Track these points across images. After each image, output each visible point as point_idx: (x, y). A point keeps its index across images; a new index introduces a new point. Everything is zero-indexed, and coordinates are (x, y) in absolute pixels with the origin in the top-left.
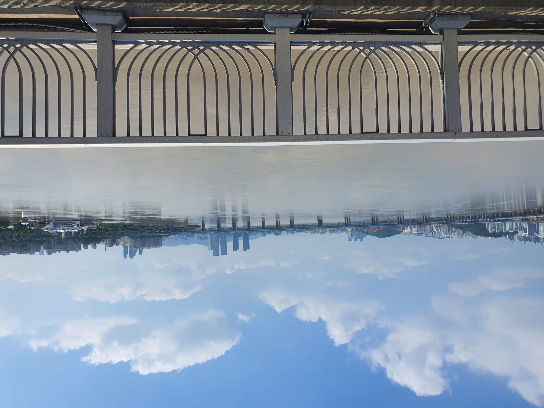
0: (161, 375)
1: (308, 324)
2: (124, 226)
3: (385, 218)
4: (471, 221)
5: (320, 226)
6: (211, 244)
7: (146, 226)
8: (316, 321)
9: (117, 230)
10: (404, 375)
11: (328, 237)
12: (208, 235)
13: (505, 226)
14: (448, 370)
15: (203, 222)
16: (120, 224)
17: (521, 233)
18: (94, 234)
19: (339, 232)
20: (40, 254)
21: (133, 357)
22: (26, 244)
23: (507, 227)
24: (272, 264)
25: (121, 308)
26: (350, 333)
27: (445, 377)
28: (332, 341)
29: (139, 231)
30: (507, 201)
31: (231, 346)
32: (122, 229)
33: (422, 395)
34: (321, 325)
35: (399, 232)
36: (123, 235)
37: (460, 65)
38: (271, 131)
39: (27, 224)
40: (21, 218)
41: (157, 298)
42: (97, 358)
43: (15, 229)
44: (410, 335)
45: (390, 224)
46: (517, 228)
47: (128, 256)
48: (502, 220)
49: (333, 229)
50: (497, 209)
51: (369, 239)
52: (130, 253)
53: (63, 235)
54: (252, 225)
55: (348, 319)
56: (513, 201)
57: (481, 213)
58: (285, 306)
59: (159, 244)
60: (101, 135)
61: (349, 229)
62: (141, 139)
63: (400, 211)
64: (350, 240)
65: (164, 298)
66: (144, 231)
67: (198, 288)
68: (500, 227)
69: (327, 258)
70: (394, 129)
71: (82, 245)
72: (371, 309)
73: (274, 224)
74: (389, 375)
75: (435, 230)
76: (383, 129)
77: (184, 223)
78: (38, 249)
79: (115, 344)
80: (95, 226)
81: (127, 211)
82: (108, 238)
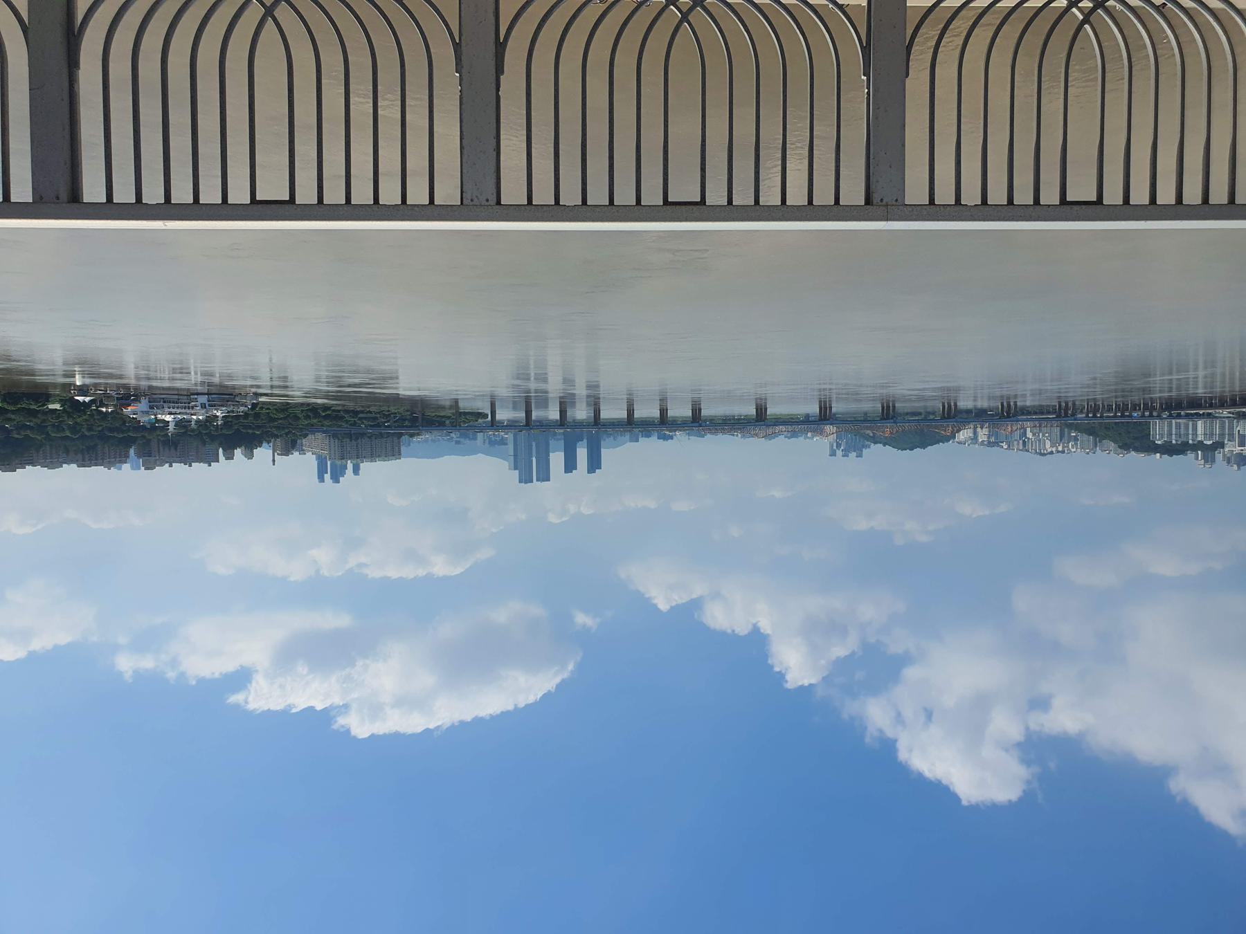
0: (396, 737)
1: (726, 640)
2: (313, 410)
3: (916, 405)
4: (1115, 416)
5: (760, 420)
6: (515, 456)
7: (362, 412)
8: (746, 632)
9: (297, 418)
10: (939, 759)
11: (781, 446)
12: (509, 436)
13: (1195, 428)
14: (1034, 748)
15: (493, 405)
16: (302, 404)
17: (1232, 447)
18: (245, 427)
19: (809, 435)
20: (133, 468)
21: (337, 700)
22: (96, 445)
23: (1199, 432)
24: (652, 504)
25: (315, 591)
26: (823, 662)
27: (1027, 762)
28: (781, 676)
29: (347, 422)
30: (1205, 368)
31: (558, 680)
32: (308, 417)
33: (973, 801)
34: (757, 641)
35: (946, 439)
36: (312, 429)
37: (909, 48)
38: (853, 194)
39: (87, 399)
40: (75, 385)
41: (393, 573)
42: (263, 697)
43: (64, 411)
44: (958, 668)
45: (925, 419)
46: (1222, 435)
47: (327, 477)
48: (1187, 416)
49: (797, 428)
50: (1179, 389)
51: (877, 452)
52: (331, 470)
53: (171, 427)
54: (606, 414)
55: (818, 630)
56: (1219, 371)
57: (1136, 398)
58: (679, 598)
59: (395, 453)
60: (41, 198)
61: (829, 428)
62: (348, 210)
63: (949, 389)
64: (833, 454)
65: (409, 572)
66: (360, 423)
67: (485, 553)
68: (1182, 431)
69: (777, 494)
70: (1140, 196)
71: (221, 450)
72: (871, 610)
73: (623, 414)
74: (903, 755)
75: (1029, 435)
76: (1113, 196)
77: (451, 407)
78: (123, 458)
79: (302, 668)
80: (242, 409)
81: (275, 375)
82: (277, 436)
